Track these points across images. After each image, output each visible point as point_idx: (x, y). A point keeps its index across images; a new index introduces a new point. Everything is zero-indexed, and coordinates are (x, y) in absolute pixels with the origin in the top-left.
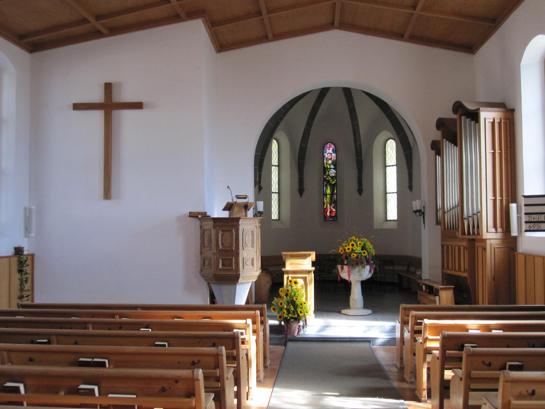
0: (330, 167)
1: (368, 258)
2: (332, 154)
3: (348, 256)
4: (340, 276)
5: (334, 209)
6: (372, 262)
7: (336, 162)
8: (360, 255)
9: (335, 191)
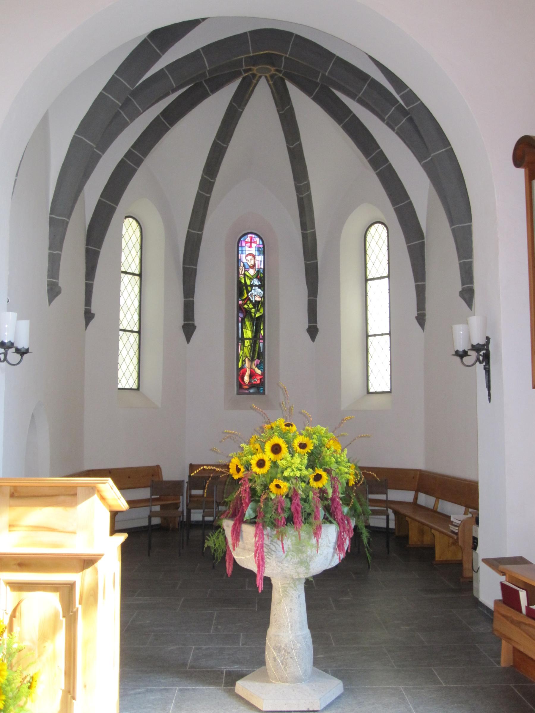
0: (251, 282)
1: (330, 495)
2: (257, 257)
3: (259, 489)
4: (234, 559)
5: (258, 368)
6: (346, 509)
7: (264, 274)
8: (303, 485)
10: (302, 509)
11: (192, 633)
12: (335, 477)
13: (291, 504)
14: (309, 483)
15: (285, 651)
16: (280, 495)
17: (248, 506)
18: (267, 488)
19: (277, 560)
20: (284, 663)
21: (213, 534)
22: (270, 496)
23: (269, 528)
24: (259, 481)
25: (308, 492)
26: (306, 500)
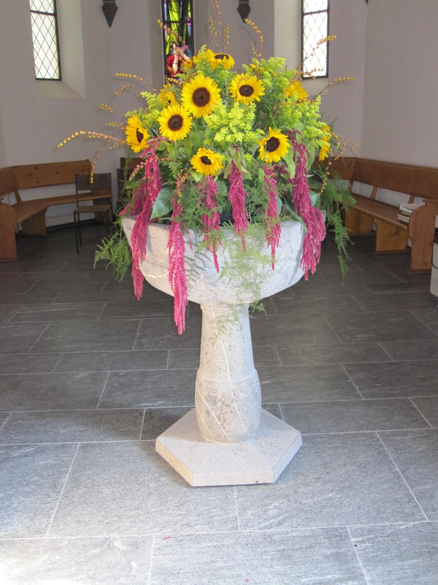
1: (292, 176)
3: (173, 166)
6: (314, 198)
9: (189, 14)
10: (246, 198)
11: (110, 351)
12: (302, 144)
13: (228, 190)
14: (257, 154)
15: (223, 403)
16: (210, 175)
17: (157, 196)
18: (188, 164)
19: (207, 281)
20: (222, 419)
21: (107, 240)
22: (193, 178)
23: (191, 232)
24: (172, 153)
25: (257, 171)
26: (252, 183)
